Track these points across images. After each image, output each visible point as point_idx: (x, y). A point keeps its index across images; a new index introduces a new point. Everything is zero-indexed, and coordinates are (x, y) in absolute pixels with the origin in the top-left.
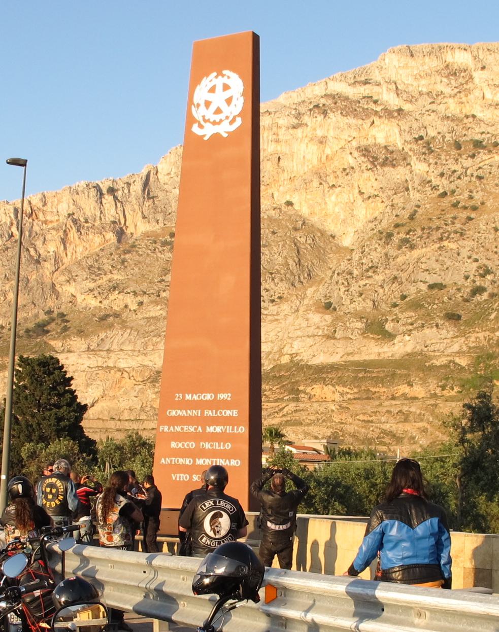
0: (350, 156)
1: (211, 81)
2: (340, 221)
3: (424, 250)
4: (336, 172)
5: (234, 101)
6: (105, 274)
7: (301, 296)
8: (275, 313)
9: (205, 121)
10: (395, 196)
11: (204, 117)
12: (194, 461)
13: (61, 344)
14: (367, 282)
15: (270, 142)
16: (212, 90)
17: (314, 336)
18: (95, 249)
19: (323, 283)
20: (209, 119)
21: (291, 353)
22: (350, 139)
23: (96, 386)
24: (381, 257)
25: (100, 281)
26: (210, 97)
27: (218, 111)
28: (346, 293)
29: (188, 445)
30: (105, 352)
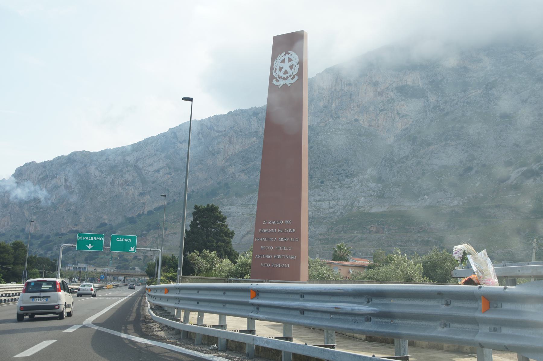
0: (392, 92)
1: (282, 57)
3: (436, 146)
5: (294, 67)
6: (251, 161)
8: (349, 183)
9: (279, 78)
10: (418, 115)
11: (279, 75)
12: (273, 256)
14: (402, 165)
17: (371, 196)
18: (246, 147)
19: (377, 166)
21: (359, 206)
24: (410, 151)
26: (282, 65)
27: (286, 72)
29: (269, 248)
30: (251, 206)
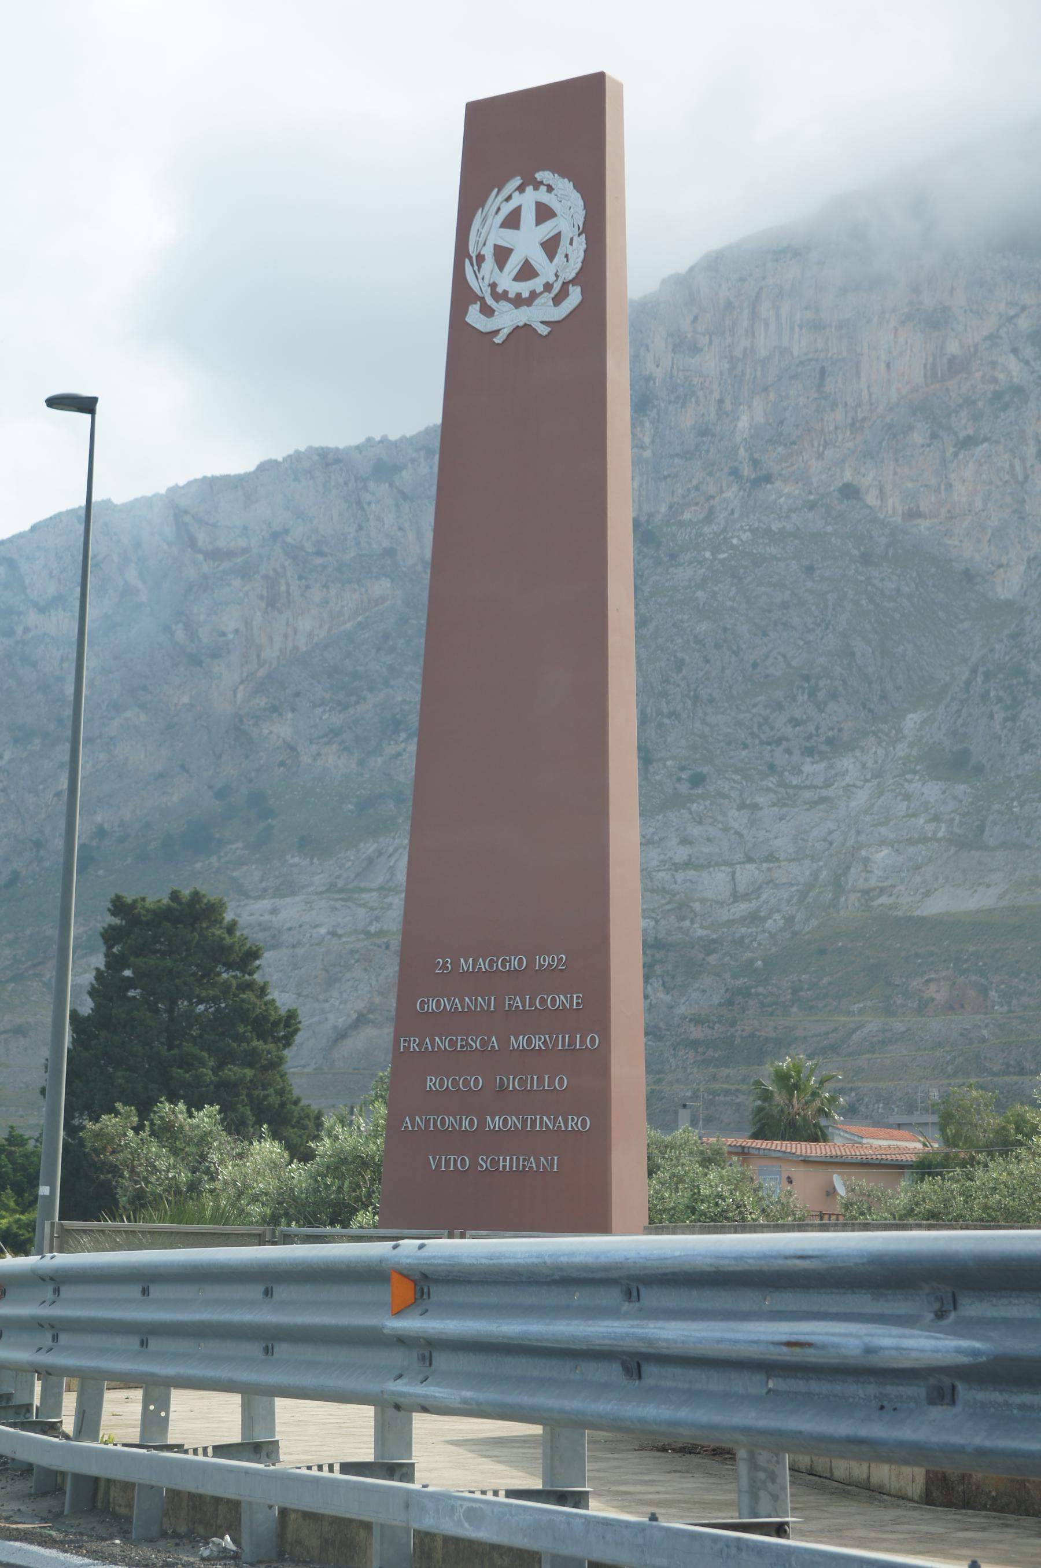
0: (1012, 356)
2: (990, 531)
4: (974, 403)
5: (564, 247)
7: (887, 735)
8: (819, 781)
9: (498, 297)
11: (493, 286)
13: (257, 876)
15: (797, 329)
16: (513, 221)
17: (924, 839)
20: (506, 292)
22: (1012, 313)
23: (350, 983)
25: (359, 708)
26: (506, 238)
27: (527, 272)
28: (1008, 724)
29: (466, 1082)
